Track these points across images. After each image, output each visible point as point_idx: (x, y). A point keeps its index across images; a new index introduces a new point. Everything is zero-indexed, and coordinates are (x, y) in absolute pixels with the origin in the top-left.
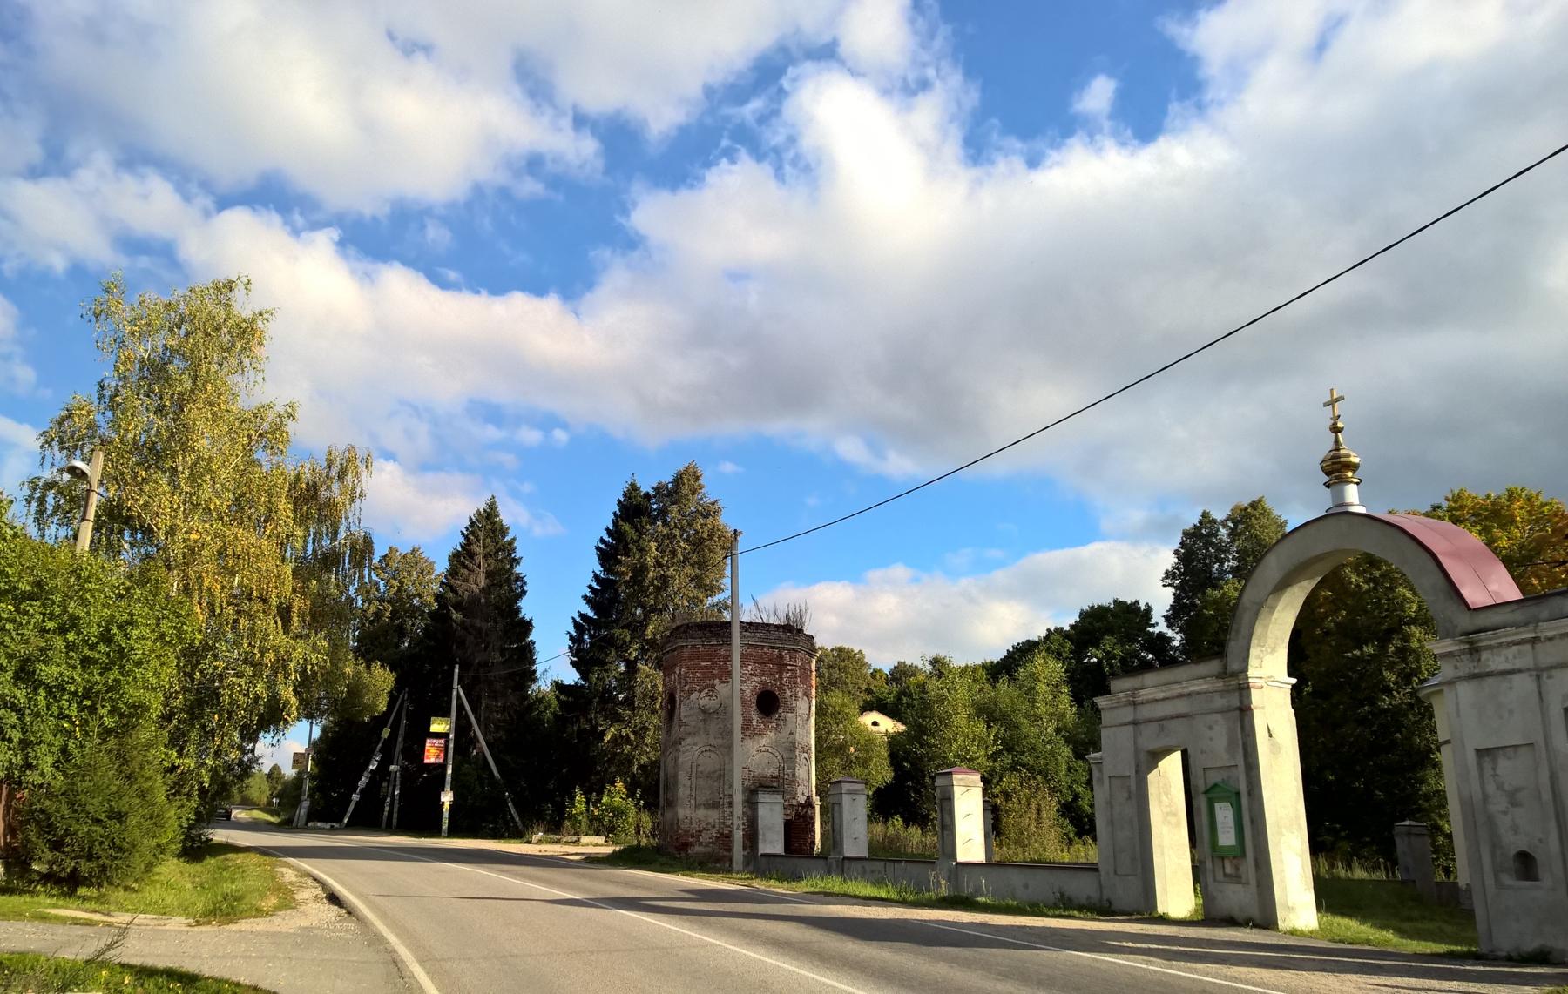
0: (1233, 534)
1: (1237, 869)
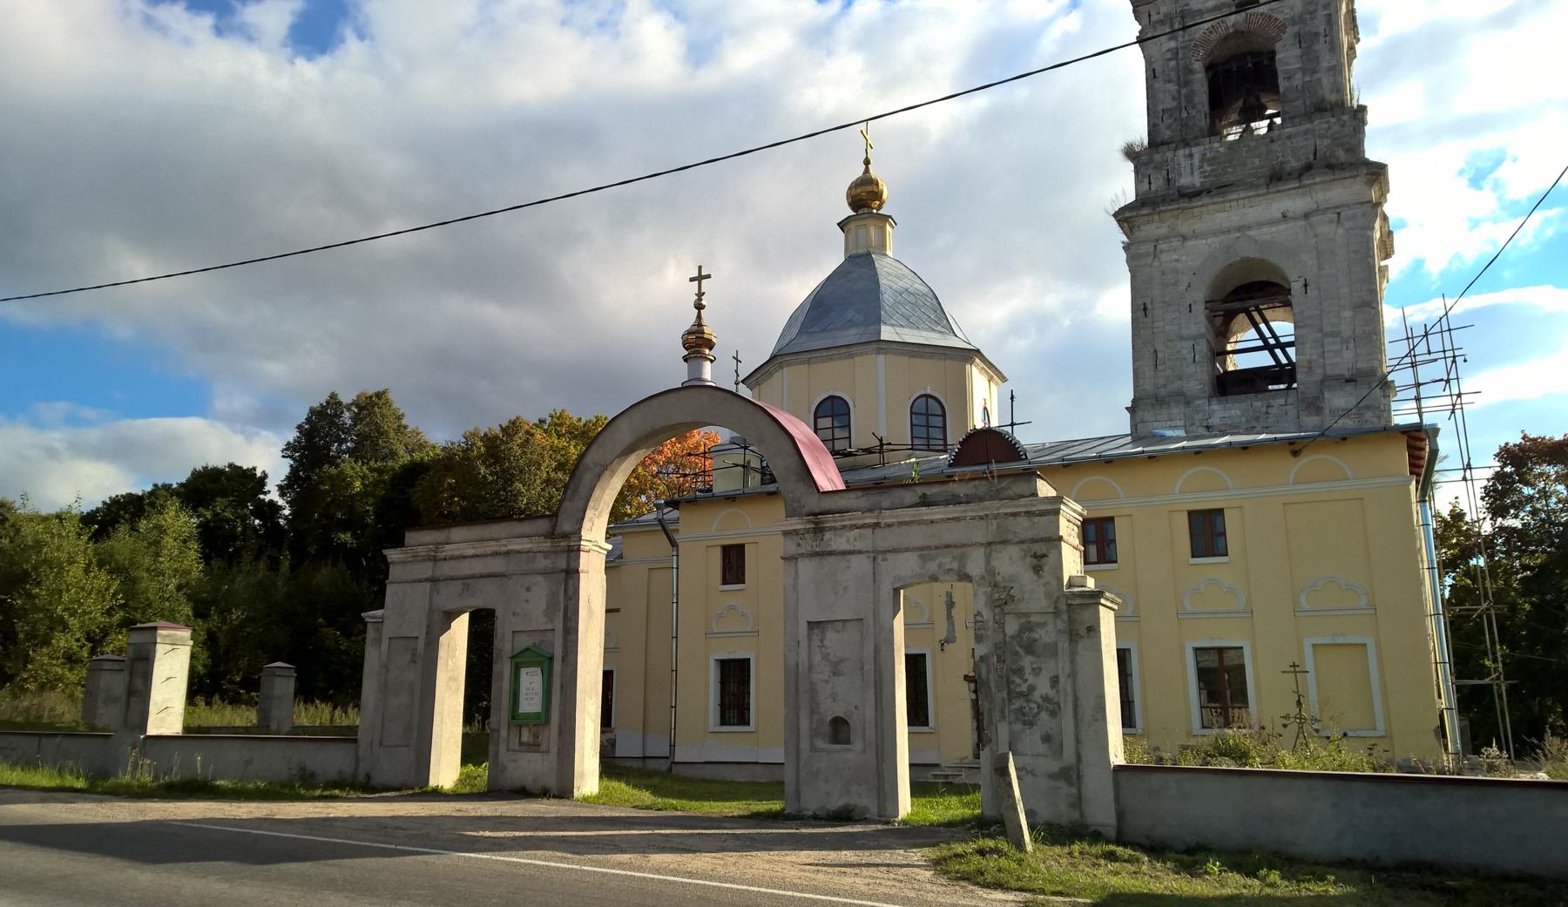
0: (356, 419)
1: (536, 736)
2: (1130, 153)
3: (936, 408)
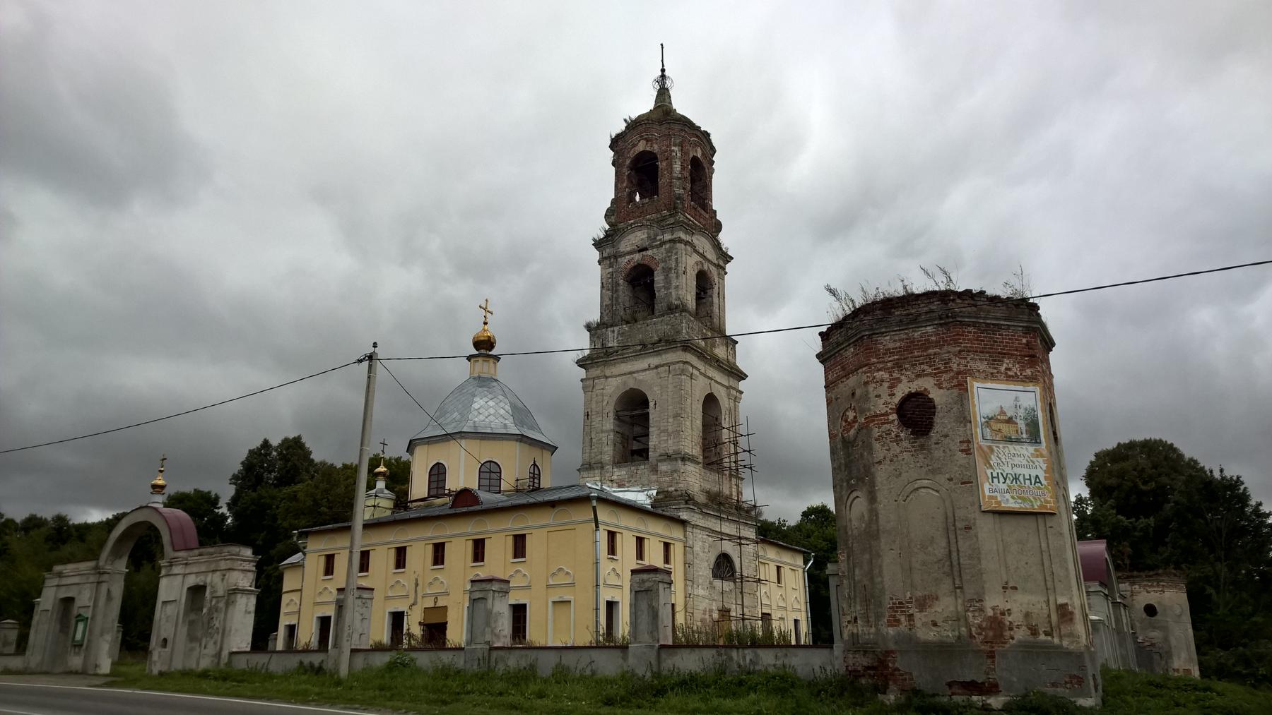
2: (589, 327)
3: (494, 468)
